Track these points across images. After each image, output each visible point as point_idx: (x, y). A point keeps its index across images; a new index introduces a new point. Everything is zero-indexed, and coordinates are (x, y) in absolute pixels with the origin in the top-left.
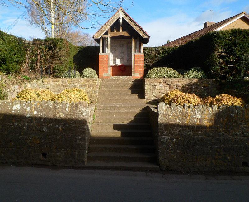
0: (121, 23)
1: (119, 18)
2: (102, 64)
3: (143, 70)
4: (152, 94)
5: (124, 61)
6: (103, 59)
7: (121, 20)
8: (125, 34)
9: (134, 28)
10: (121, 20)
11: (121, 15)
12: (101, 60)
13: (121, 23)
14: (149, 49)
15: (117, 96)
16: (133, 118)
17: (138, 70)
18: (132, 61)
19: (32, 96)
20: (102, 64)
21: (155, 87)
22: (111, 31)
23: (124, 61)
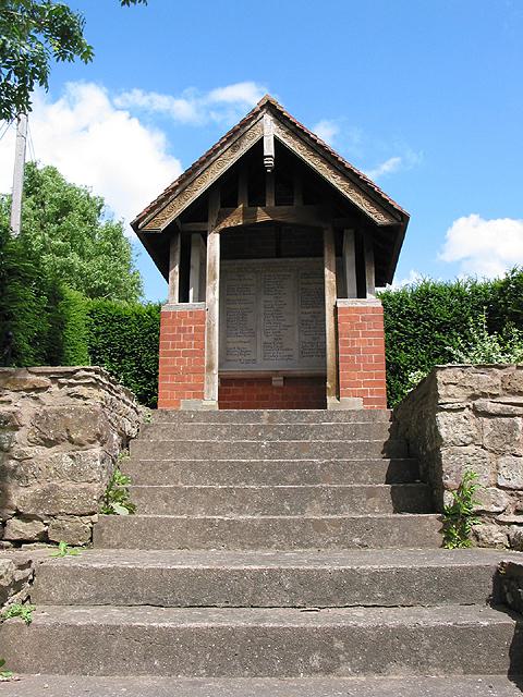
0: (269, 162)
1: (261, 141)
2: (177, 353)
3: (380, 383)
4: (497, 473)
5: (286, 353)
6: (180, 330)
7: (269, 149)
8: (289, 214)
9: (332, 181)
10: (269, 149)
11: (269, 130)
12: (170, 338)
13: (269, 162)
14: (401, 299)
15: (166, 499)
16: (507, 220)
17: (358, 384)
18: (325, 356)
19: (519, 519)
20: (177, 353)
21: (515, 424)
22: (222, 207)
23: (286, 353)
